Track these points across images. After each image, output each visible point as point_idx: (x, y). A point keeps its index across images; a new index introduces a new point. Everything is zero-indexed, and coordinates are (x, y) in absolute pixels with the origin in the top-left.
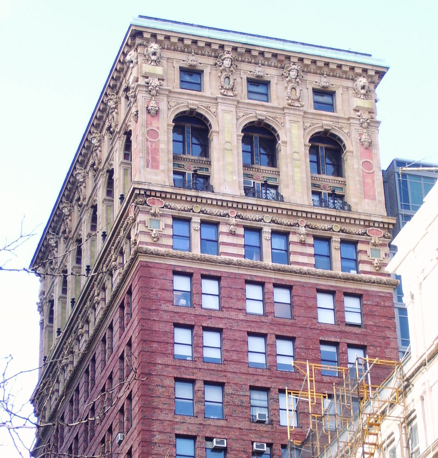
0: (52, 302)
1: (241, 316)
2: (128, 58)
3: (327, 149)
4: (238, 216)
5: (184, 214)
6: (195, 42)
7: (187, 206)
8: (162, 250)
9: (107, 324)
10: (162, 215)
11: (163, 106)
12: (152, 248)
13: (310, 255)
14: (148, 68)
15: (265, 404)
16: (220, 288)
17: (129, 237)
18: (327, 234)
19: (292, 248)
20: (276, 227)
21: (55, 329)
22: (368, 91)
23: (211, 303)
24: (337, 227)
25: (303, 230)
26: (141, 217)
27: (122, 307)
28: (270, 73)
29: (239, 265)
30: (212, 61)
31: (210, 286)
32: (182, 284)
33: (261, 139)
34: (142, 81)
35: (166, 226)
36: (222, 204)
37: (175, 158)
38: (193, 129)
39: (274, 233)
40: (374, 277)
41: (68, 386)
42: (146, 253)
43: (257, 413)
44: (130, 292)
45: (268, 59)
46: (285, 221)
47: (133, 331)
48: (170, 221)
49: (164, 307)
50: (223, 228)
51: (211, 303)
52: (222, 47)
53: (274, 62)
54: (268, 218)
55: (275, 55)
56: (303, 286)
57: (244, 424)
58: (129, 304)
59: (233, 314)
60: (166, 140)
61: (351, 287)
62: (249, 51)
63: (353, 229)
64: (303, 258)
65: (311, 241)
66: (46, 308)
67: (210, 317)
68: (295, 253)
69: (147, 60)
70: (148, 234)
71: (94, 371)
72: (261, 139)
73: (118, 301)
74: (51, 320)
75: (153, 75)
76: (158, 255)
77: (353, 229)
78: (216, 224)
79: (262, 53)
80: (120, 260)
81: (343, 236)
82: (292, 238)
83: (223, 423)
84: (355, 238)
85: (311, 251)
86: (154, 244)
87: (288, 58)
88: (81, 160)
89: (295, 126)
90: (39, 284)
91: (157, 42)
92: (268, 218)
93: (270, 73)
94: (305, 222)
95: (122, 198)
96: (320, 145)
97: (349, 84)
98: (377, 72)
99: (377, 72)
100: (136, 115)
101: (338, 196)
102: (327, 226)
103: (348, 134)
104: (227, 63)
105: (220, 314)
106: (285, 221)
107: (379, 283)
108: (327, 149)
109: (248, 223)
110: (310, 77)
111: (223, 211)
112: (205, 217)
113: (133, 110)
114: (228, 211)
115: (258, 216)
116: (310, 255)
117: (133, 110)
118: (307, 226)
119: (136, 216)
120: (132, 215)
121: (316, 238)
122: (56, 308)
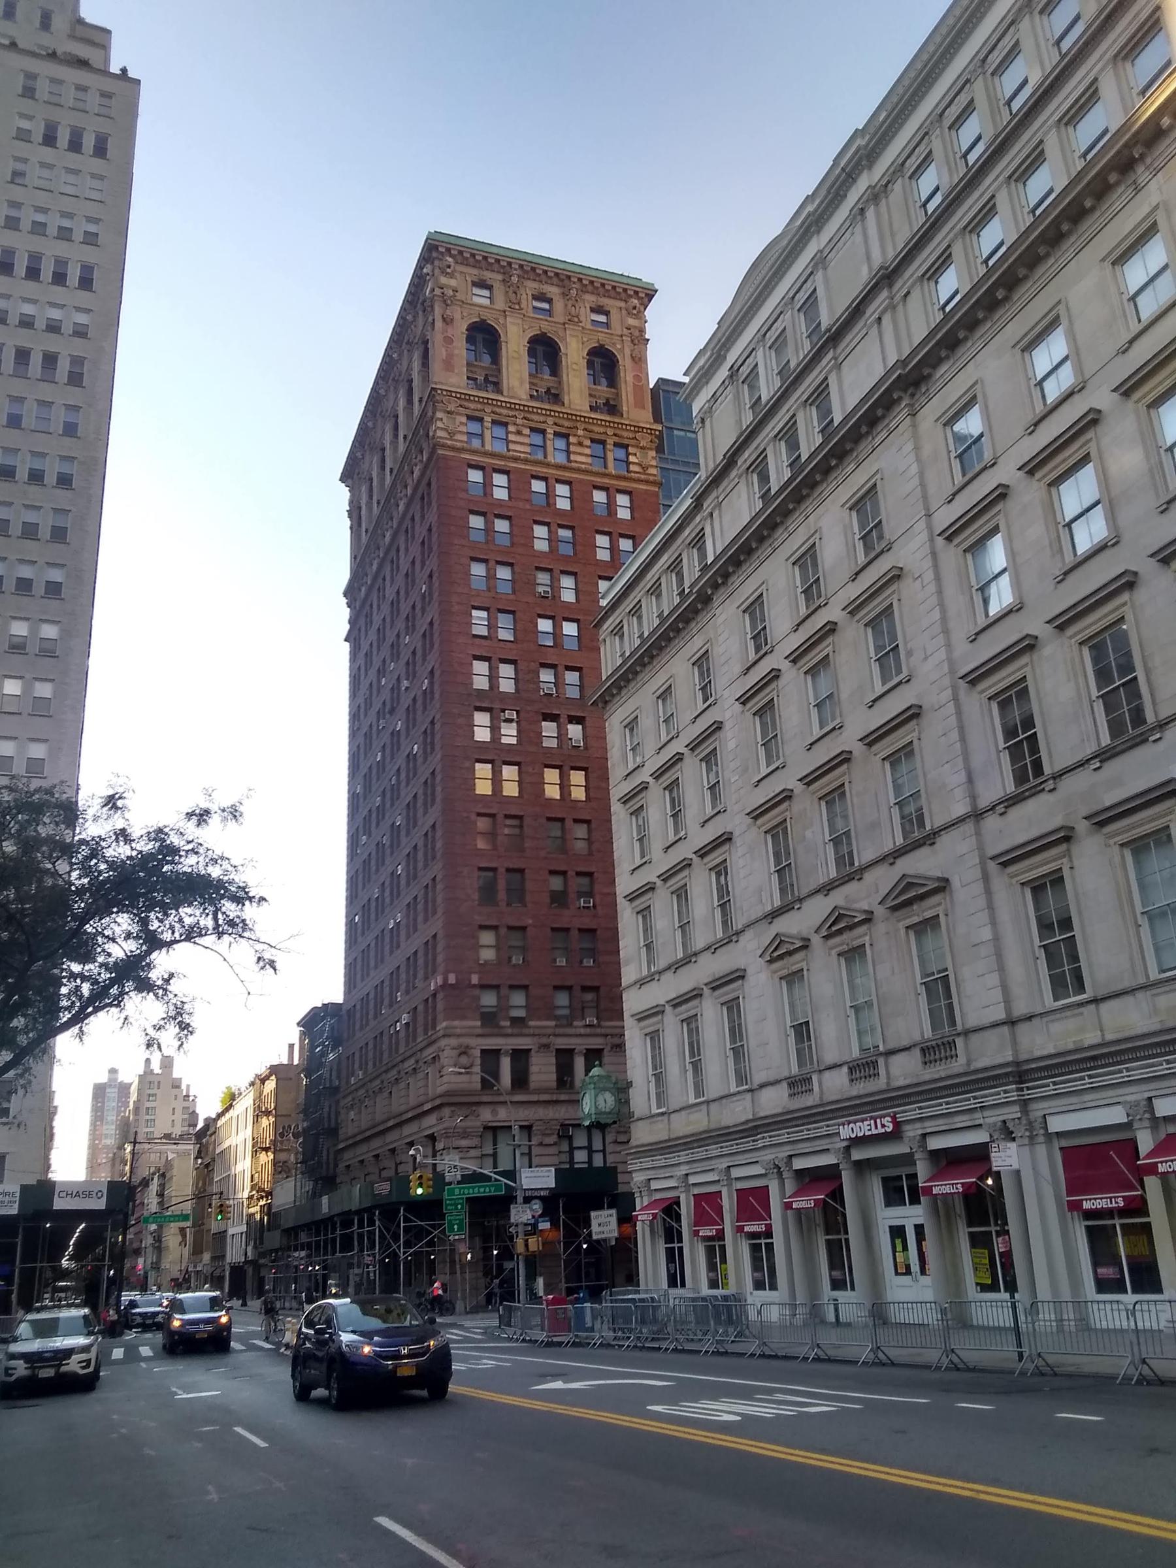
0: (360, 508)
1: (528, 507)
2: (425, 270)
3: (603, 363)
4: (525, 418)
5: (477, 414)
6: (485, 258)
7: (479, 406)
8: (459, 445)
9: (409, 516)
10: (458, 414)
11: (457, 316)
12: (449, 442)
13: (587, 455)
14: (444, 280)
15: (549, 582)
16: (509, 481)
17: (428, 435)
18: (602, 437)
19: (572, 448)
20: (558, 429)
21: (364, 529)
22: (639, 312)
23: (501, 494)
24: (610, 432)
25: (580, 432)
26: (439, 415)
27: (423, 498)
28: (553, 291)
29: (526, 461)
30: (500, 277)
31: (500, 480)
32: (475, 476)
33: (545, 351)
34: (438, 291)
35: (461, 423)
36: (512, 407)
37: (468, 364)
38: (484, 339)
39: (556, 434)
40: (643, 477)
41: (375, 579)
42: (444, 446)
43: (540, 589)
44: (429, 484)
45: (550, 278)
46: (566, 424)
47: (432, 517)
48: (464, 419)
49: (461, 495)
50: (511, 428)
51: (501, 494)
52: (510, 264)
53: (555, 280)
54: (550, 421)
55: (557, 274)
56: (581, 481)
57: (531, 599)
58: (429, 494)
59: (521, 504)
60: (461, 348)
61: (623, 484)
62: (533, 269)
63: (625, 434)
64: (582, 457)
65: (588, 443)
66: (355, 515)
67: (501, 506)
68: (574, 453)
69: (443, 272)
70: (446, 430)
71: (398, 559)
72: (545, 351)
73: (419, 494)
74: (360, 525)
75: (448, 287)
76: (453, 448)
77: (625, 434)
78: (506, 425)
79: (545, 272)
80: (419, 457)
81: (616, 439)
82: (572, 439)
83: (512, 597)
84: (626, 442)
85: (588, 451)
86: (451, 439)
87: (569, 277)
88: (333, 1308)
89: (574, 340)
90: (349, 494)
91: (451, 256)
92: (550, 421)
93: (553, 291)
94: (583, 426)
95: (421, 400)
96: (596, 360)
97: (622, 304)
98: (647, 295)
99: (647, 295)
100: (433, 323)
101: (612, 408)
102: (602, 430)
103: (622, 350)
104: (515, 279)
105: (510, 504)
106: (566, 424)
107: (647, 482)
108: (603, 363)
109: (533, 425)
110: (588, 297)
111: (511, 413)
112: (496, 417)
113: (430, 319)
114: (516, 413)
115: (542, 419)
116: (587, 455)
117: (430, 319)
118: (585, 429)
119: (434, 413)
120: (430, 414)
121: (592, 441)
122: (363, 512)
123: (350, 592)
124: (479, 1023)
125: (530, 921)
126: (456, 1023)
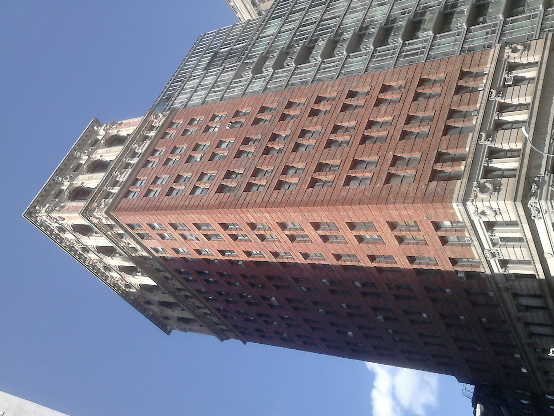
49: (134, 202)
123: (222, 335)
124: (459, 181)
125: (391, 153)
126: (455, 196)
